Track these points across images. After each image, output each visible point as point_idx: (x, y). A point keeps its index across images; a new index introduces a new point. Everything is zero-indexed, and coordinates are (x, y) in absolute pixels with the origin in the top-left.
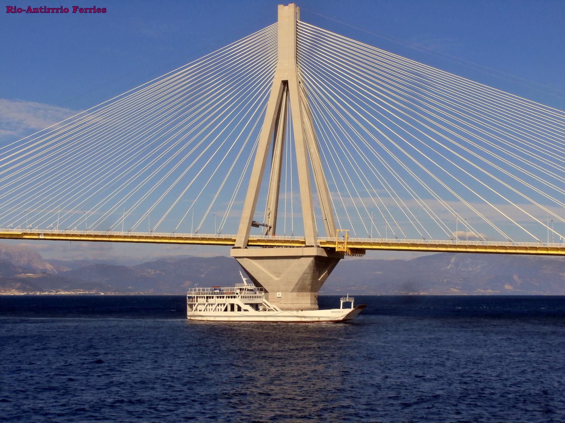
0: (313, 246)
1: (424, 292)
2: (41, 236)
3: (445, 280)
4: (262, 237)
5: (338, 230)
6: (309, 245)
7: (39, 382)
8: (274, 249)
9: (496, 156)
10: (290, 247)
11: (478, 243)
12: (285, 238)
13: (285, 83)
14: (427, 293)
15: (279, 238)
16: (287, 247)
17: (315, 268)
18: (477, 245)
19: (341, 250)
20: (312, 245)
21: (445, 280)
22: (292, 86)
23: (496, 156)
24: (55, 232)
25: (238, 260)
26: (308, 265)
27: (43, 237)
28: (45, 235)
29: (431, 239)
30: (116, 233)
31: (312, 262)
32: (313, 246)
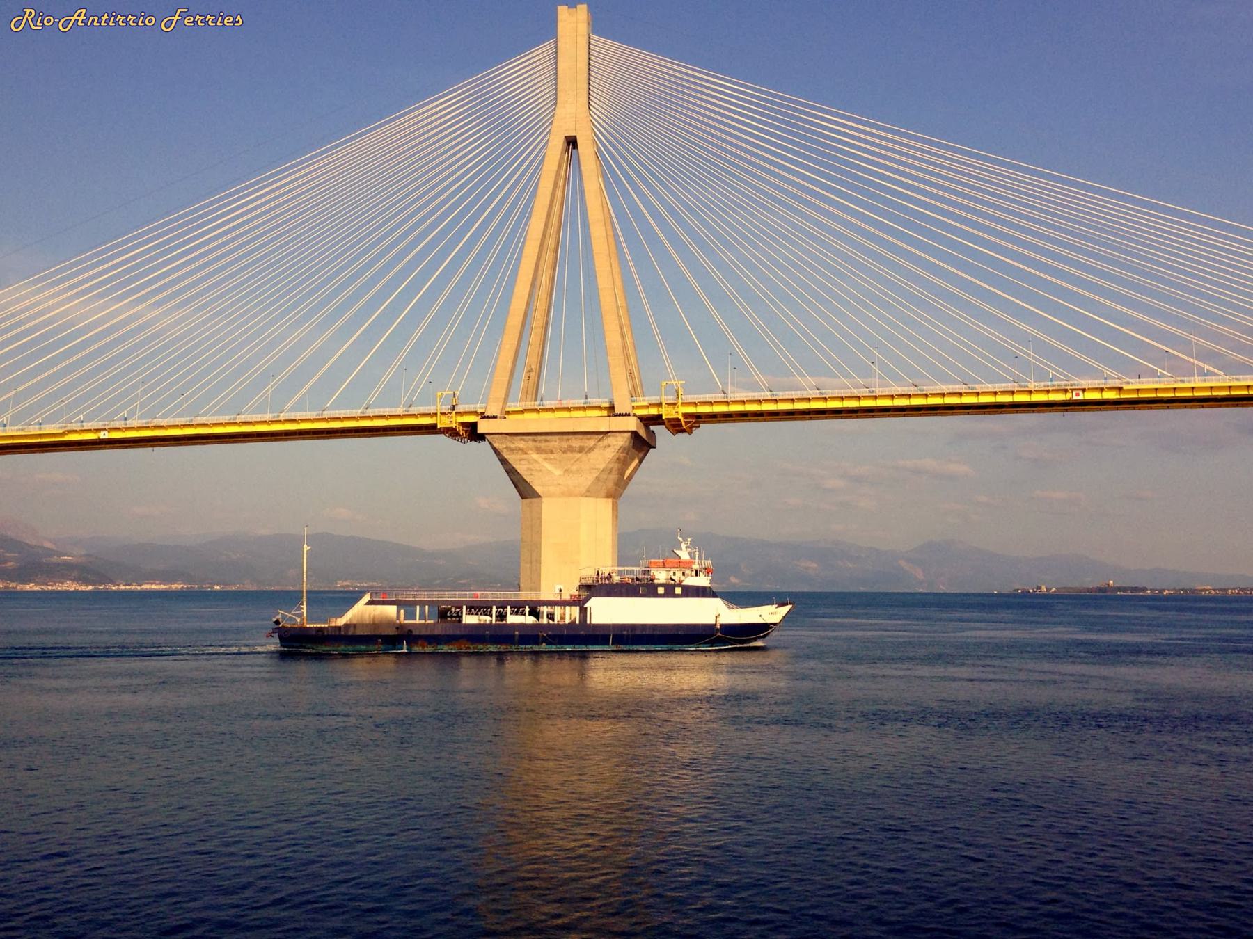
0: (629, 415)
13: (572, 142)
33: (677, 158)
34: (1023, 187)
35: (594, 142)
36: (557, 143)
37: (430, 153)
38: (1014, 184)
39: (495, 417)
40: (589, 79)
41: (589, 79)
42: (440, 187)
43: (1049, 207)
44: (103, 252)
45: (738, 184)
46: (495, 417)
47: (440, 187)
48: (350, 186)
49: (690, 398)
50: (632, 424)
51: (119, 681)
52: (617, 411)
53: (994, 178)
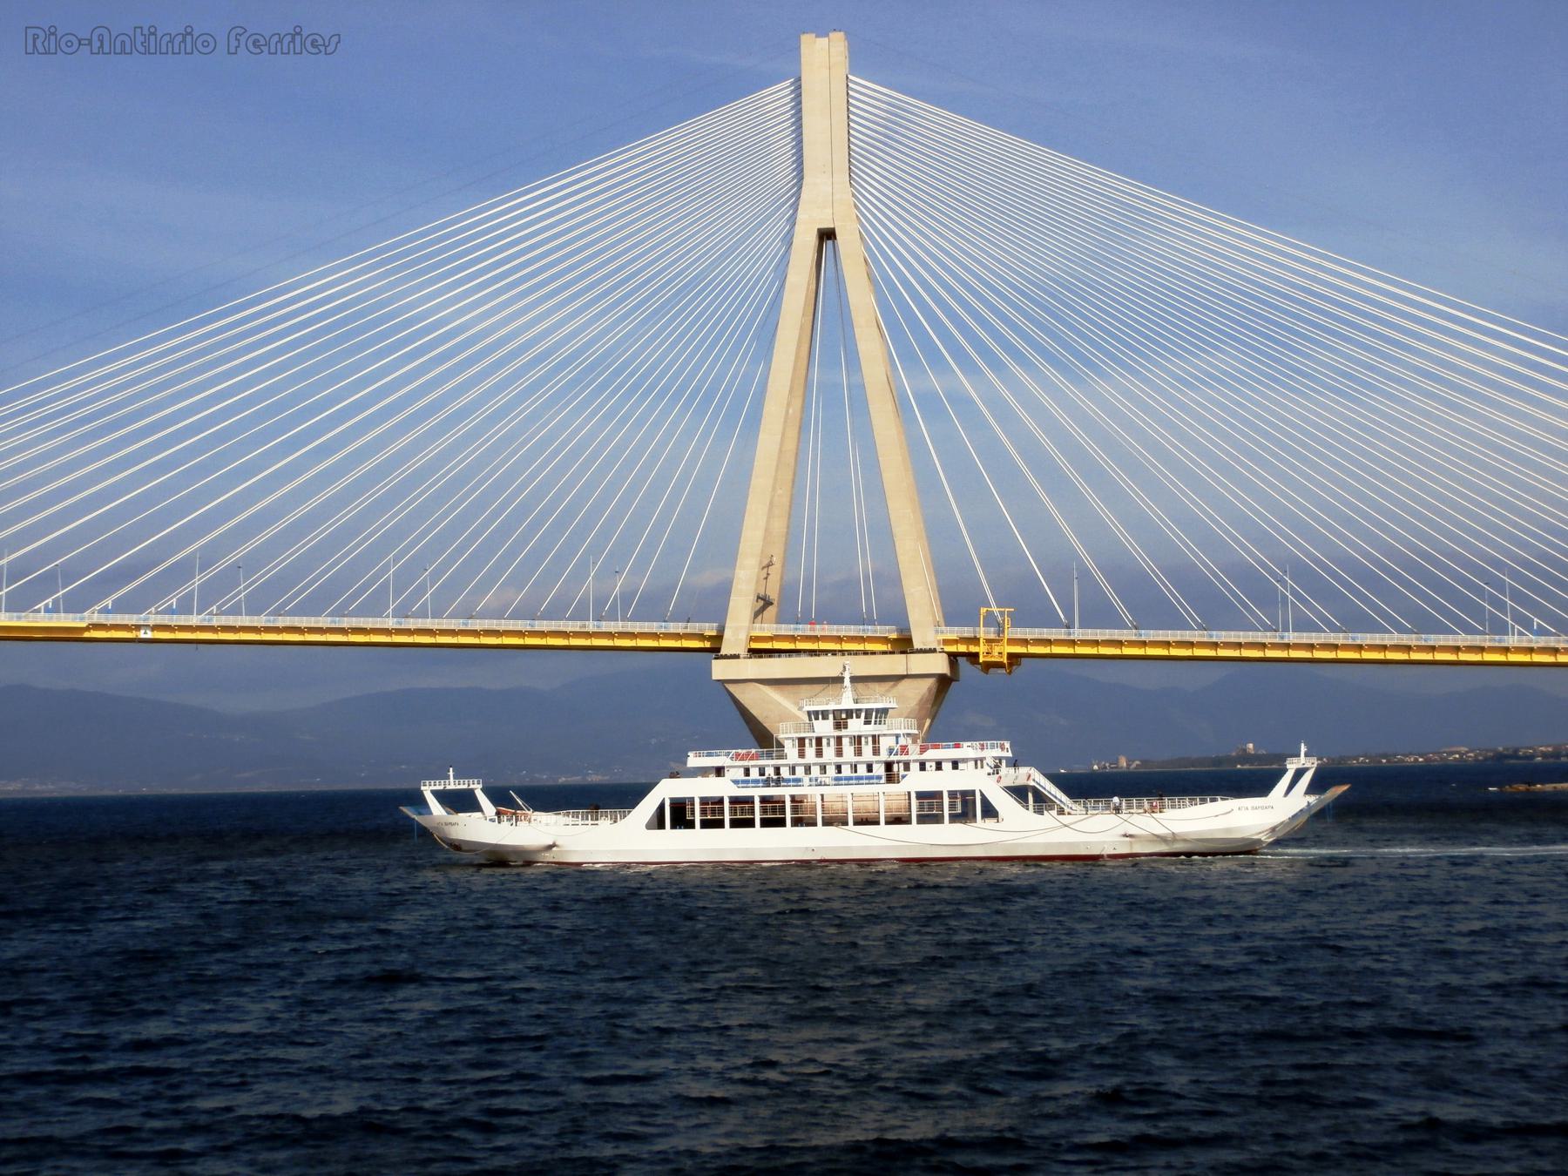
0: (933, 651)
1: (597, 774)
2: (142, 631)
3: (653, 741)
4: (332, 622)
5: (985, 609)
6: (923, 647)
7: (770, 1023)
8: (822, 659)
9: (1463, 400)
10: (865, 653)
11: (640, 627)
12: (876, 631)
13: (827, 235)
14: (606, 778)
15: (466, 624)
16: (856, 654)
17: (917, 707)
18: (502, 628)
19: (993, 660)
20: (932, 647)
21: (653, 741)
22: (847, 241)
23: (1463, 400)
24: (409, 623)
25: (727, 685)
26: (919, 697)
27: (150, 635)
28: (156, 628)
29: (1325, 632)
30: (838, 630)
31: (930, 690)
32: (933, 651)
33: (1167, 296)
34: (1028, 258)
35: (862, 238)
36: (806, 240)
37: (652, 248)
38: (1187, 275)
39: (736, 657)
40: (848, 109)
41: (848, 109)
42: (890, 214)
43: (1021, 268)
44: (736, 257)
45: (1402, 392)
46: (736, 657)
47: (890, 214)
48: (1061, 189)
49: (1020, 633)
50: (940, 665)
51: (204, 1047)
52: (917, 645)
53: (1234, 281)
